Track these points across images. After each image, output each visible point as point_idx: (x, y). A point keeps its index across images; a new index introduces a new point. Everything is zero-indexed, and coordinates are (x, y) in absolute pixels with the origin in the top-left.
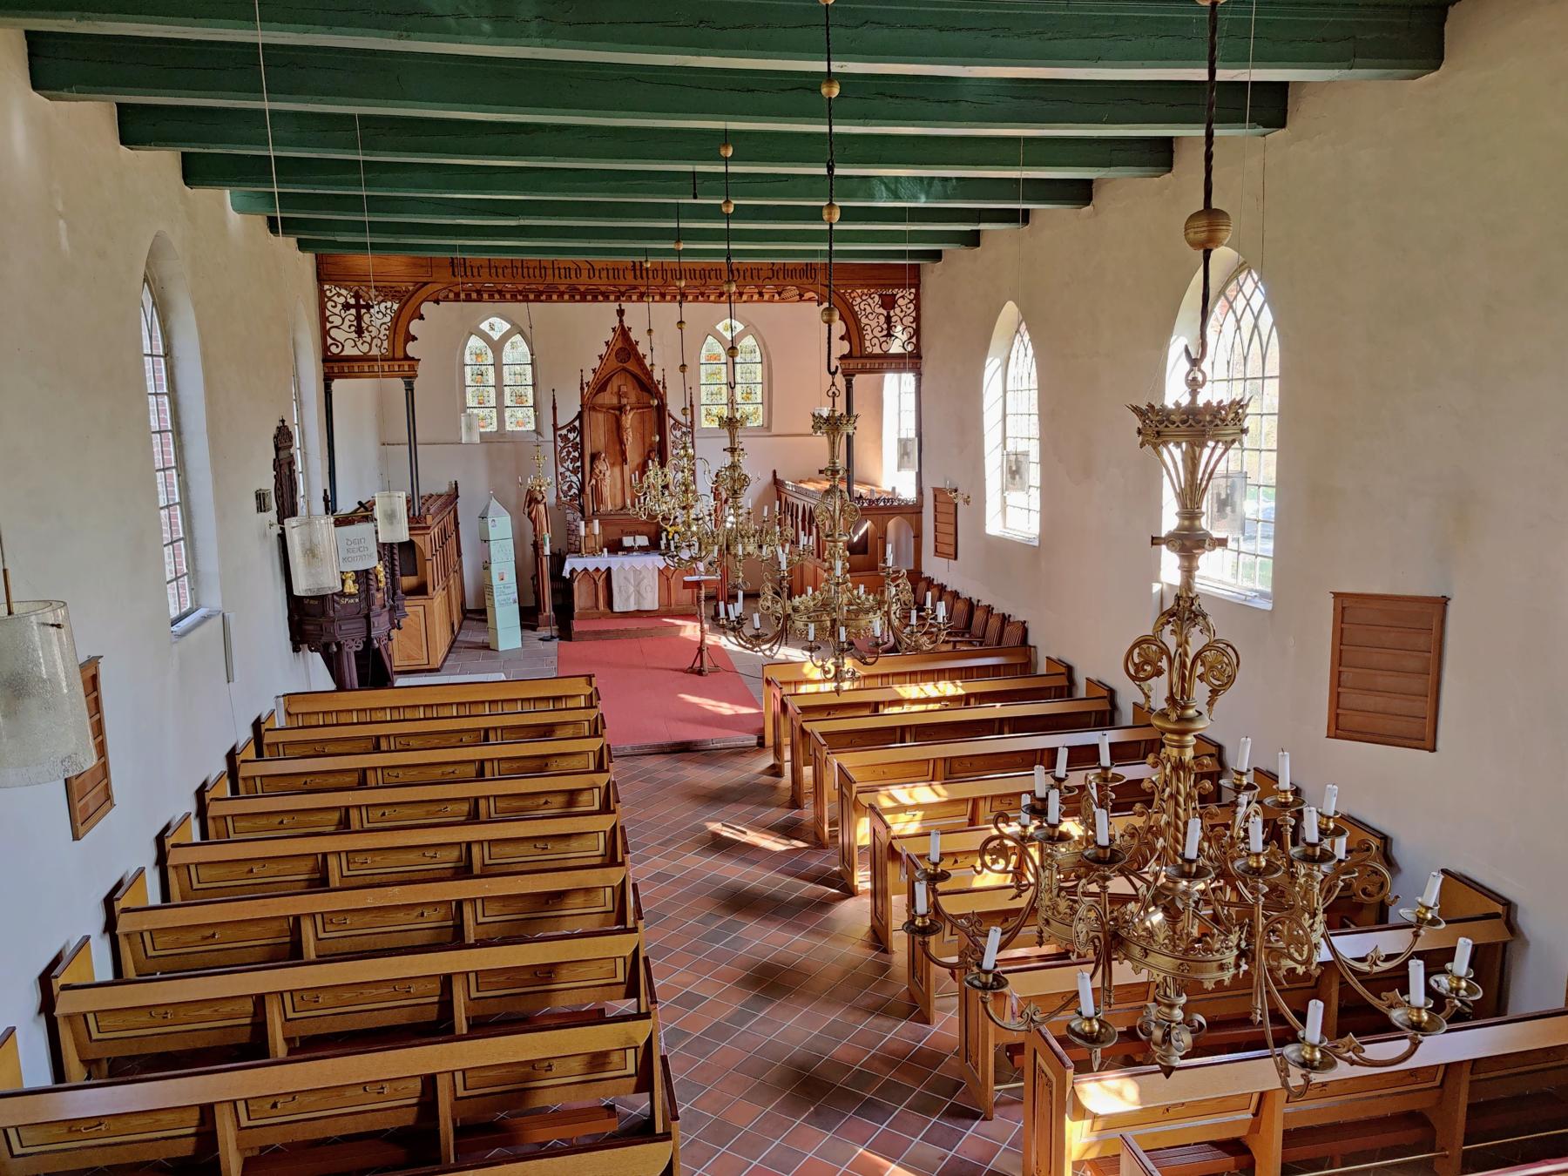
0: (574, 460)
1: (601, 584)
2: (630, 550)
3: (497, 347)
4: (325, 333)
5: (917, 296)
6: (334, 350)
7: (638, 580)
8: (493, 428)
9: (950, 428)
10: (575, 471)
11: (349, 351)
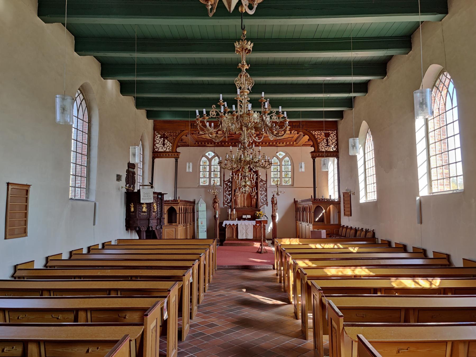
0: (229, 191)
1: (234, 230)
2: (245, 219)
3: (210, 160)
4: (154, 145)
5: (337, 133)
6: (156, 150)
7: (246, 229)
8: (208, 184)
9: (348, 171)
10: (229, 195)
11: (160, 150)
